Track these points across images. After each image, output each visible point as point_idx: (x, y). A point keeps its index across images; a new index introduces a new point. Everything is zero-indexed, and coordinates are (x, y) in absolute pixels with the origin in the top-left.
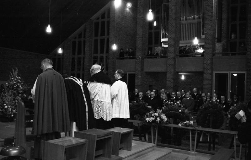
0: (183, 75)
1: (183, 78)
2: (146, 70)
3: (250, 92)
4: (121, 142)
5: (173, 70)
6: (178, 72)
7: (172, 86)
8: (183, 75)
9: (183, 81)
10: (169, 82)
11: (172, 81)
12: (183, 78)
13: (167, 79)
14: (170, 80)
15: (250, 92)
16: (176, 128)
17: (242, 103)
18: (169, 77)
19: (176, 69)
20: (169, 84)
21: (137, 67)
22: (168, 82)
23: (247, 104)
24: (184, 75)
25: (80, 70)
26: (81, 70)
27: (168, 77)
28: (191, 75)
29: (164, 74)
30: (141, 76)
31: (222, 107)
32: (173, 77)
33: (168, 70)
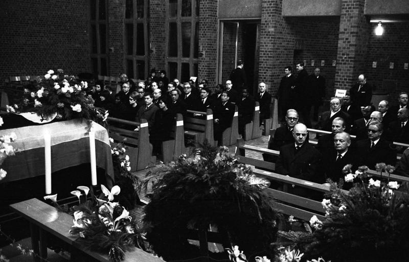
0: (380, 25)
1: (379, 31)
2: (287, 11)
3: (408, 206)
4: (110, 191)
5: (356, 12)
6: (369, 17)
7: (352, 55)
8: (380, 25)
9: (380, 40)
10: (344, 42)
11: (353, 40)
12: (379, 31)
13: (340, 36)
14: (347, 39)
15: (408, 206)
16: (33, 219)
17: (93, 109)
18: (345, 30)
19: (365, 9)
20: (344, 48)
21: (265, 5)
22: (341, 43)
23: (338, 205)
24: (383, 24)
25: (142, 16)
26: (145, 16)
27: (342, 30)
28: (396, 23)
29: (333, 21)
30: (275, 27)
31: (333, 114)
32: (355, 30)
33: (344, 11)
